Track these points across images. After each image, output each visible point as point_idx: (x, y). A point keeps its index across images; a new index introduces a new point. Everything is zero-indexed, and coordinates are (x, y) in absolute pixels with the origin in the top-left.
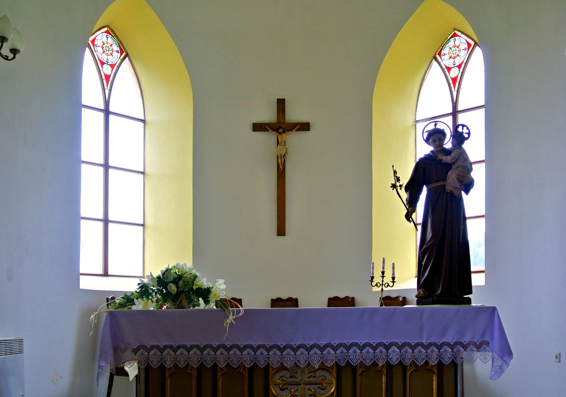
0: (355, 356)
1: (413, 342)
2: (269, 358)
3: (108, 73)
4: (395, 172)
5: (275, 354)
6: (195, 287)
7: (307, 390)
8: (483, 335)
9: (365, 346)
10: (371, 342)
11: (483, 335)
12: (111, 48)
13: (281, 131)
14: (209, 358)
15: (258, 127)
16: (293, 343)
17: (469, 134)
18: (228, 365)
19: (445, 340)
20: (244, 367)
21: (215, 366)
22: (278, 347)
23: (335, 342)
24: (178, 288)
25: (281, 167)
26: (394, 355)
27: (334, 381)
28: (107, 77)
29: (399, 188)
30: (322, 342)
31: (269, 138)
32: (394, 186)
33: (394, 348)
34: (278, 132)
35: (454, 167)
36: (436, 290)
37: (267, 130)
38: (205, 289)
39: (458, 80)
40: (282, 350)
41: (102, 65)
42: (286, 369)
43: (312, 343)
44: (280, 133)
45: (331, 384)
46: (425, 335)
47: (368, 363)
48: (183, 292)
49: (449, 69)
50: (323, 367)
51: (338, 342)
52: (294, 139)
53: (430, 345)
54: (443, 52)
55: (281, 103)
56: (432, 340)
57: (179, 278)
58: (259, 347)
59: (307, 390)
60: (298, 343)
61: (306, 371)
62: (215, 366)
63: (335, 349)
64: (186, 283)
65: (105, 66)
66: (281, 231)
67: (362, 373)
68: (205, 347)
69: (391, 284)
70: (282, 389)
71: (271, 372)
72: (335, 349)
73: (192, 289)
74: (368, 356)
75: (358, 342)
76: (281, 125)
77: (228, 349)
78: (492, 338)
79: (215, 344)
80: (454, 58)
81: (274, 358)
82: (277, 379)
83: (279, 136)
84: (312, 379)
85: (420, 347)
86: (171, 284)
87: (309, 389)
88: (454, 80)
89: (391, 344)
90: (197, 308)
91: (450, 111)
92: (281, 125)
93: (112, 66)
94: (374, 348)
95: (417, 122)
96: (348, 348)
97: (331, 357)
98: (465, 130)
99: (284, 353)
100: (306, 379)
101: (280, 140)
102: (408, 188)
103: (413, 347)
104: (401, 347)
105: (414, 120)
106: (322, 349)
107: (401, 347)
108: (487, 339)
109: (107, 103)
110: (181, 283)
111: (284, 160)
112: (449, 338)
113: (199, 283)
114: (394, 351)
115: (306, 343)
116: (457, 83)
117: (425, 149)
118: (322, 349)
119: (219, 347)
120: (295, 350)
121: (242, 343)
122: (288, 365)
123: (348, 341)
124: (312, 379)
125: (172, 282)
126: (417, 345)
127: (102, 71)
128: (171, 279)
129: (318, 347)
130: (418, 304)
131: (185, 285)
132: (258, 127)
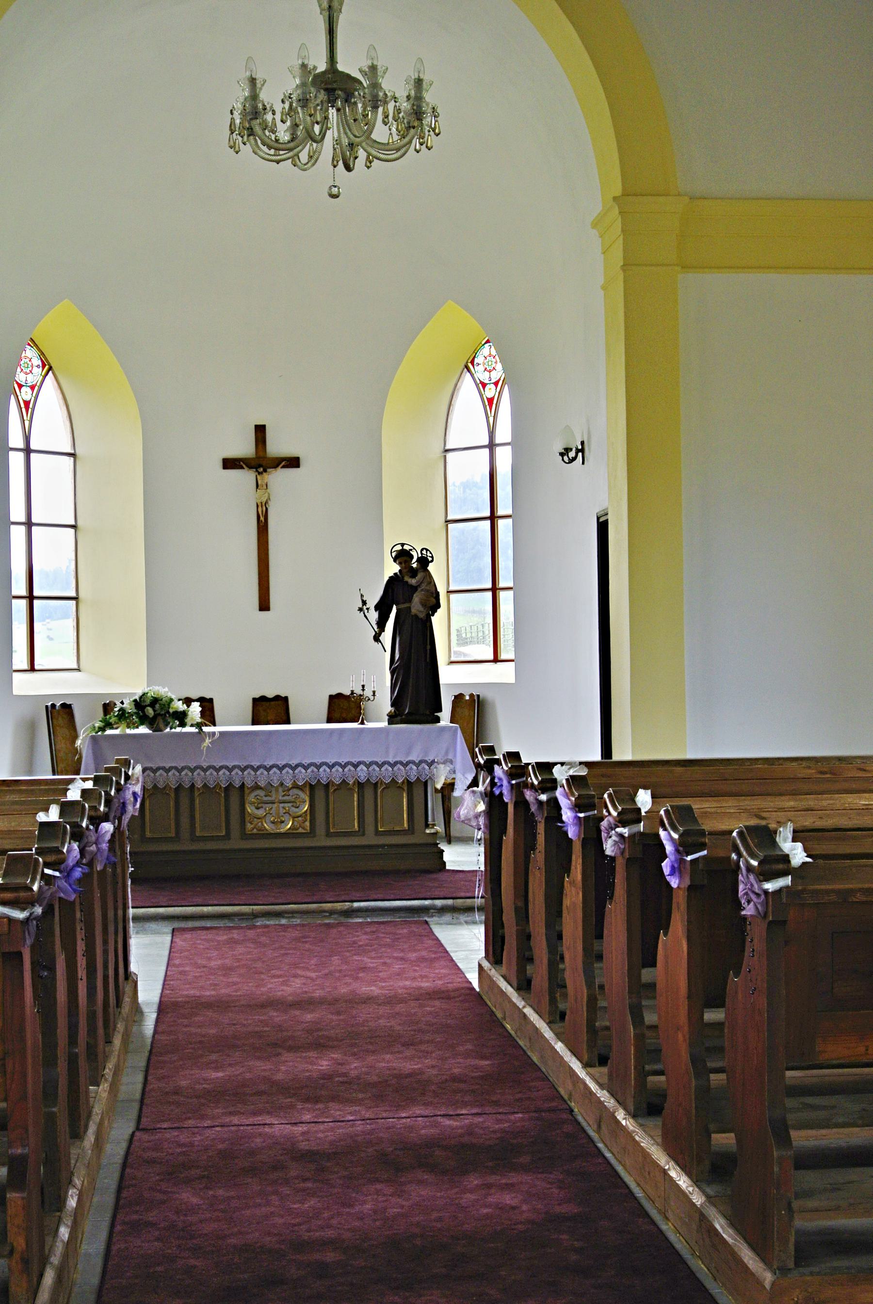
0: (324, 774)
1: (380, 760)
2: (243, 778)
3: (27, 398)
4: (362, 596)
5: (249, 774)
6: (171, 711)
7: (281, 809)
8: (447, 753)
9: (333, 765)
10: (340, 761)
11: (447, 753)
12: (30, 364)
13: (261, 470)
14: (186, 778)
15: (229, 464)
16: (265, 764)
17: (432, 557)
18: (205, 786)
19: (410, 758)
20: (221, 787)
21: (193, 786)
22: (252, 767)
23: (306, 762)
24: (154, 711)
25: (262, 518)
26: (362, 773)
27: (307, 799)
28: (27, 404)
29: (366, 611)
30: (294, 762)
31: (245, 477)
32: (361, 610)
33: (362, 767)
34: (257, 471)
35: (419, 589)
36: (405, 710)
37: (242, 468)
38: (181, 712)
39: (495, 402)
40: (256, 770)
41: (20, 389)
42: (261, 788)
43: (284, 763)
44: (259, 473)
45: (305, 802)
46: (390, 756)
47: (337, 781)
48: (159, 714)
49: (484, 385)
50: (295, 786)
51: (308, 762)
52: (278, 478)
53: (396, 763)
54: (476, 361)
55: (260, 431)
56: (398, 759)
57: (155, 701)
58: (234, 767)
59: (281, 809)
60: (271, 763)
61: (280, 789)
62: (193, 786)
63: (306, 768)
64: (163, 707)
65: (23, 389)
66: (264, 605)
67: (335, 790)
68: (183, 768)
69: (372, 698)
70: (258, 808)
71: (247, 791)
72: (306, 768)
73: (168, 712)
74: (336, 775)
75: (328, 761)
76: (261, 460)
77: (205, 770)
78: (455, 756)
79: (192, 765)
80: (490, 371)
81: (249, 778)
82: (251, 798)
83: (259, 477)
84: (286, 798)
85: (386, 766)
86: (149, 708)
87: (284, 808)
88: (491, 401)
89: (360, 763)
90: (173, 730)
91: (487, 442)
92: (261, 460)
93: (32, 388)
94: (343, 767)
95: (447, 451)
96: (318, 767)
97: (303, 776)
98: (429, 554)
99: (258, 773)
100: (280, 798)
101: (259, 482)
102: (377, 608)
103: (380, 766)
104: (368, 766)
105: (442, 449)
106: (294, 768)
107: (368, 766)
108: (450, 757)
109: (27, 439)
110: (157, 706)
111: (267, 509)
112: (414, 757)
113: (175, 706)
114: (362, 770)
115: (278, 763)
116: (494, 406)
117: (393, 568)
118: (294, 768)
119: (196, 768)
120: (268, 769)
121: (218, 764)
122: (262, 784)
123: (318, 761)
124: (286, 798)
125: (149, 706)
126: (384, 763)
127: (20, 398)
128: (148, 702)
129: (290, 766)
130: (390, 722)
131: (162, 709)
132: (229, 464)
